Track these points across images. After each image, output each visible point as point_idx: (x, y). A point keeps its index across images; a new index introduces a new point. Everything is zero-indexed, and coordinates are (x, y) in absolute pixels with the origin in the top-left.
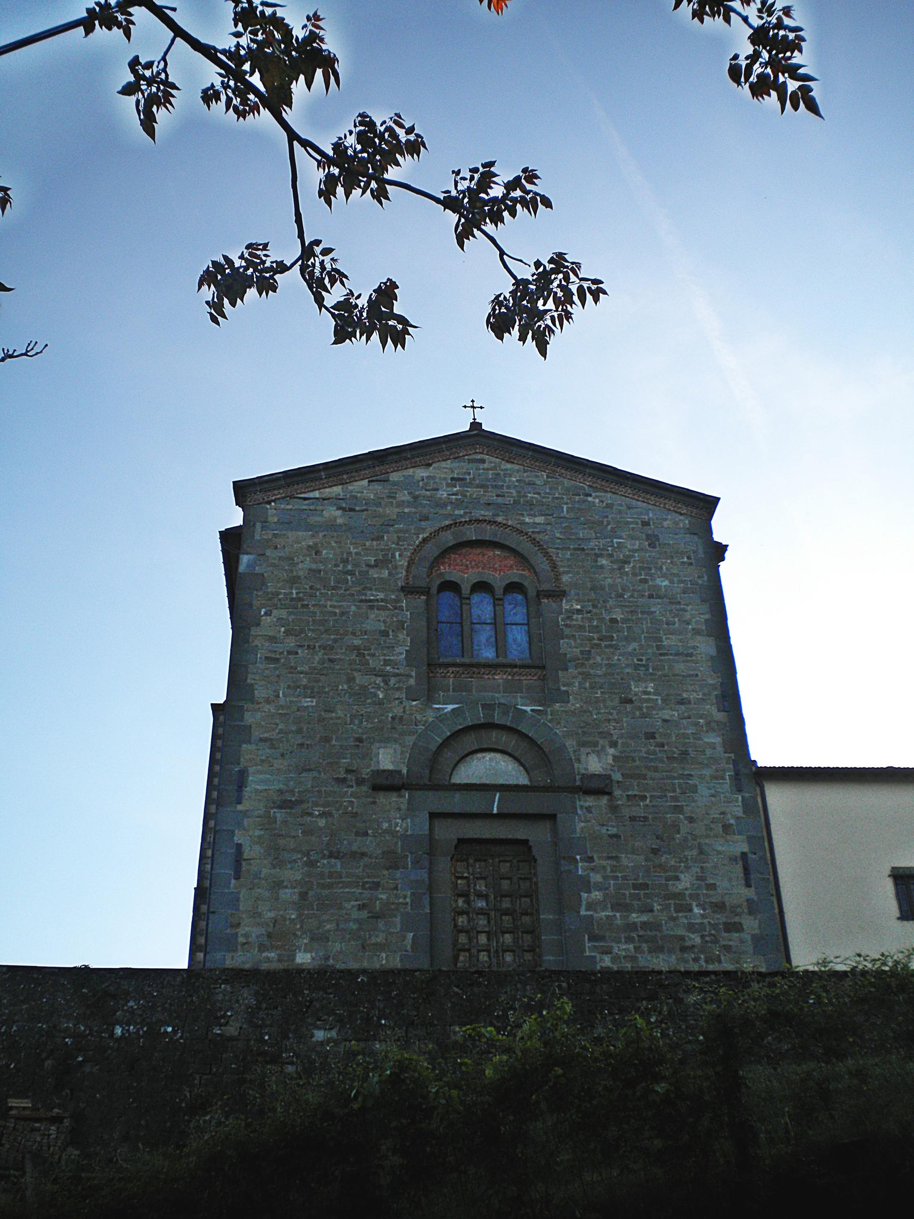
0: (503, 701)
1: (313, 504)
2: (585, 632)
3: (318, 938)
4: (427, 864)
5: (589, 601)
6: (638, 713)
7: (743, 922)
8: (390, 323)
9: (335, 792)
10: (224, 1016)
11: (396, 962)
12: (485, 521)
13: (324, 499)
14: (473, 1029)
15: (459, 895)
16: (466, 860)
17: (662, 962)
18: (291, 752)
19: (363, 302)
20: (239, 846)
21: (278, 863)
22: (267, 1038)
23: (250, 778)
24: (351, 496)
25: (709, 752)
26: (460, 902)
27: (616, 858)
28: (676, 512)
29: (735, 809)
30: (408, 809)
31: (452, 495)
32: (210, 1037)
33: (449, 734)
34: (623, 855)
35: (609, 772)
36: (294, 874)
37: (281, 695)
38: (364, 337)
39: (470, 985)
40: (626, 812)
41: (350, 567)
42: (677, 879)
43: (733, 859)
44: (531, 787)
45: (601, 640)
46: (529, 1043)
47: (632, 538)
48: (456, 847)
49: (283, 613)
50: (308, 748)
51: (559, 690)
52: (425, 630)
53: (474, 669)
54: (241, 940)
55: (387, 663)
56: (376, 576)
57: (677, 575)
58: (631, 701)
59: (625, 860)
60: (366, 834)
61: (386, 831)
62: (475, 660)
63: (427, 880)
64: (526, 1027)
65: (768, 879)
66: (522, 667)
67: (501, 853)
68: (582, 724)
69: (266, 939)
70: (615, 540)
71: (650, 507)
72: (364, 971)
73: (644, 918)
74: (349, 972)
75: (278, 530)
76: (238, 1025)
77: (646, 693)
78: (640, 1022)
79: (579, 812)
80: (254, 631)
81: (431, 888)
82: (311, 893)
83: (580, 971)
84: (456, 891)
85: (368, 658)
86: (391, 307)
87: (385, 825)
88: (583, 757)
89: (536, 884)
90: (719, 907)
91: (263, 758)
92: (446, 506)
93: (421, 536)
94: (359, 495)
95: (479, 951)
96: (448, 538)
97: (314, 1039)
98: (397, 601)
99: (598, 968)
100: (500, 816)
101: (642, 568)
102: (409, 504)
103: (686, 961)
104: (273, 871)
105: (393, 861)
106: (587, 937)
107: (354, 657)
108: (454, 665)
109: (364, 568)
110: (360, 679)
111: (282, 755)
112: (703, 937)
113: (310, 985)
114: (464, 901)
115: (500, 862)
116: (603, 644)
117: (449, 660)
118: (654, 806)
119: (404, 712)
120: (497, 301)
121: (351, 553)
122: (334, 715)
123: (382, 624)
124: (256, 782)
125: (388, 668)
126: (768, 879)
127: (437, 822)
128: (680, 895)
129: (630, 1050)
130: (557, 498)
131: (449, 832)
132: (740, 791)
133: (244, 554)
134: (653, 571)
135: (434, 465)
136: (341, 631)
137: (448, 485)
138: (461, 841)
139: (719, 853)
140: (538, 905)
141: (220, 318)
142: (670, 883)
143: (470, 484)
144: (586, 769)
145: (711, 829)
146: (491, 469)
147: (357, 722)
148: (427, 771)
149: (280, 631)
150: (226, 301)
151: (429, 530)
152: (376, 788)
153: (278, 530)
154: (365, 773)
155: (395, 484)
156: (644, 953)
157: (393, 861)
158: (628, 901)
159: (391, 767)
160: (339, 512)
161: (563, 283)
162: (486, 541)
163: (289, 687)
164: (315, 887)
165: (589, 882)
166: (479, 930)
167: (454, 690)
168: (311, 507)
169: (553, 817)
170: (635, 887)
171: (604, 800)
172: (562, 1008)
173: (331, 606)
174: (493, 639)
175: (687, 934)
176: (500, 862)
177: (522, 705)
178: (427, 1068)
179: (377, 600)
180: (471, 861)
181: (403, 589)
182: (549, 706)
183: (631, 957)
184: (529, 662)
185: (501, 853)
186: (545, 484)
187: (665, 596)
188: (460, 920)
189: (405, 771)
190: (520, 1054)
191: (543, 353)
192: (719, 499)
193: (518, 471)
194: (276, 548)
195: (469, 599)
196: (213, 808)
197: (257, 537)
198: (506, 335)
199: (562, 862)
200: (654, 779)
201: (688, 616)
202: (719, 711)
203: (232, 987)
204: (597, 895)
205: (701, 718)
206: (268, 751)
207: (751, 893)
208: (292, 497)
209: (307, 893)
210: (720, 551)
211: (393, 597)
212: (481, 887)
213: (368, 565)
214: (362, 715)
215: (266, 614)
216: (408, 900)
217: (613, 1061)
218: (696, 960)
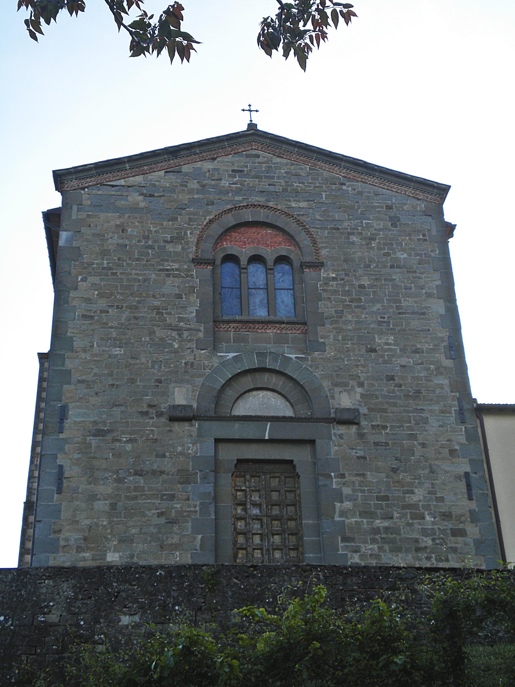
0: (272, 350)
1: (119, 190)
2: (339, 295)
3: (126, 540)
4: (212, 479)
5: (342, 270)
6: (380, 360)
7: (466, 528)
8: (177, 39)
9: (140, 422)
10: (47, 606)
11: (187, 560)
12: (259, 205)
13: (129, 187)
14: (248, 610)
15: (238, 505)
16: (244, 476)
17: (401, 560)
18: (104, 391)
19: (154, 22)
20: (61, 467)
21: (93, 480)
22: (82, 623)
23: (70, 412)
24: (150, 184)
25: (438, 391)
26: (239, 510)
27: (363, 475)
28: (414, 198)
29: (460, 437)
30: (198, 436)
31: (234, 184)
32: (35, 624)
33: (230, 376)
34: (369, 473)
35: (357, 407)
36: (105, 489)
37: (95, 346)
38: (155, 52)
39: (247, 577)
40: (372, 439)
41: (150, 243)
42: (412, 492)
43: (458, 478)
44: (295, 418)
45: (352, 302)
46: (293, 622)
47: (378, 219)
48: (236, 466)
49: (95, 279)
50: (117, 388)
51: (318, 341)
52: (212, 293)
53: (251, 325)
54: (62, 543)
55: (181, 320)
56: (171, 250)
57: (414, 249)
58: (373, 350)
59: (370, 476)
60: (164, 456)
61: (180, 453)
62: (251, 318)
63: (213, 492)
64: (291, 607)
65: (487, 494)
66: (287, 323)
67: (269, 472)
68: (336, 369)
69: (83, 542)
70: (364, 221)
71: (394, 193)
72: (162, 567)
73: (386, 524)
74: (150, 567)
75: (96, 214)
76: (59, 613)
77: (387, 344)
78: (382, 605)
79: (333, 438)
80: (72, 294)
81: (216, 498)
82: (120, 504)
83: (335, 566)
84: (237, 502)
85: (166, 316)
86: (178, 26)
87: (179, 449)
88: (336, 396)
89: (299, 495)
90: (447, 516)
91: (81, 396)
92: (228, 193)
93: (208, 218)
94: (157, 183)
95: (254, 549)
96: (230, 220)
97: (120, 623)
98: (189, 270)
99: (349, 563)
100: (271, 441)
101: (384, 244)
102: (198, 192)
103: (420, 560)
104: (88, 487)
105: (186, 477)
106: (340, 539)
107: (154, 315)
108: (235, 321)
109: (162, 244)
110: (160, 333)
111: (97, 394)
112: (433, 540)
113: (118, 579)
114: (242, 510)
115: (271, 477)
116: (353, 304)
117: (230, 318)
118: (393, 434)
119: (195, 359)
120: (266, 23)
121: (151, 231)
122: (138, 361)
123: (177, 289)
124: (74, 415)
125: (182, 324)
126: (487, 494)
127: (221, 446)
128: (413, 506)
129: (374, 627)
130: (317, 187)
131: (231, 454)
132: (463, 422)
133: (62, 231)
134: (395, 246)
135: (218, 159)
136: (144, 295)
137: (229, 176)
138: (240, 461)
139: (447, 472)
140: (301, 511)
141: (37, 34)
142: (407, 495)
143: (247, 176)
144: (339, 404)
145: (440, 453)
146: (265, 163)
147: (157, 367)
148: (213, 406)
149: (94, 294)
150: (42, 20)
151: (215, 213)
152: (173, 419)
153: (96, 214)
154: (164, 408)
155: (187, 174)
156: (386, 552)
157: (186, 477)
158: (372, 509)
159: (184, 403)
160: (141, 198)
161: (320, 7)
162: (260, 221)
163: (102, 339)
164: (123, 499)
165: (342, 494)
166: (253, 532)
167: (234, 342)
168: (119, 193)
169: (312, 442)
170: (378, 498)
171: (354, 429)
172: (319, 593)
173: (136, 274)
174: (266, 301)
175: (421, 537)
176: (271, 477)
177: (288, 354)
178: (212, 642)
179: (173, 270)
180: (248, 477)
181: (193, 260)
182: (309, 354)
183: (376, 555)
184: (294, 319)
185: (269, 472)
186: (308, 175)
187: (404, 267)
188: (239, 524)
189: (195, 406)
190: (285, 631)
191: (303, 66)
192: (449, 187)
193: (287, 164)
194: (90, 226)
195: (246, 269)
196: (39, 437)
197: (74, 217)
198: (274, 51)
199: (320, 478)
200: (393, 413)
201: (422, 282)
202: (446, 358)
203: (54, 582)
204: (348, 504)
205: (431, 364)
206: (85, 391)
207: (473, 505)
208: (102, 184)
209: (116, 504)
210: (449, 230)
211: (186, 267)
212: (255, 498)
213: (166, 242)
214: (161, 361)
215: (82, 280)
216: (198, 508)
217: (360, 637)
218: (428, 558)
